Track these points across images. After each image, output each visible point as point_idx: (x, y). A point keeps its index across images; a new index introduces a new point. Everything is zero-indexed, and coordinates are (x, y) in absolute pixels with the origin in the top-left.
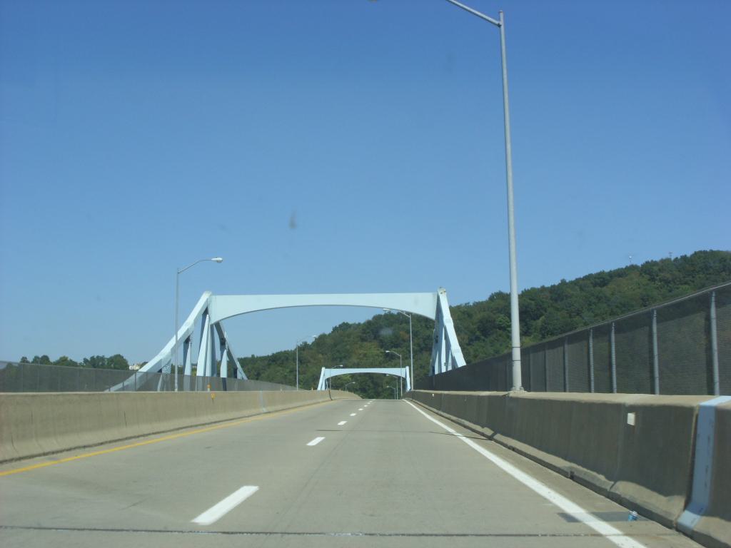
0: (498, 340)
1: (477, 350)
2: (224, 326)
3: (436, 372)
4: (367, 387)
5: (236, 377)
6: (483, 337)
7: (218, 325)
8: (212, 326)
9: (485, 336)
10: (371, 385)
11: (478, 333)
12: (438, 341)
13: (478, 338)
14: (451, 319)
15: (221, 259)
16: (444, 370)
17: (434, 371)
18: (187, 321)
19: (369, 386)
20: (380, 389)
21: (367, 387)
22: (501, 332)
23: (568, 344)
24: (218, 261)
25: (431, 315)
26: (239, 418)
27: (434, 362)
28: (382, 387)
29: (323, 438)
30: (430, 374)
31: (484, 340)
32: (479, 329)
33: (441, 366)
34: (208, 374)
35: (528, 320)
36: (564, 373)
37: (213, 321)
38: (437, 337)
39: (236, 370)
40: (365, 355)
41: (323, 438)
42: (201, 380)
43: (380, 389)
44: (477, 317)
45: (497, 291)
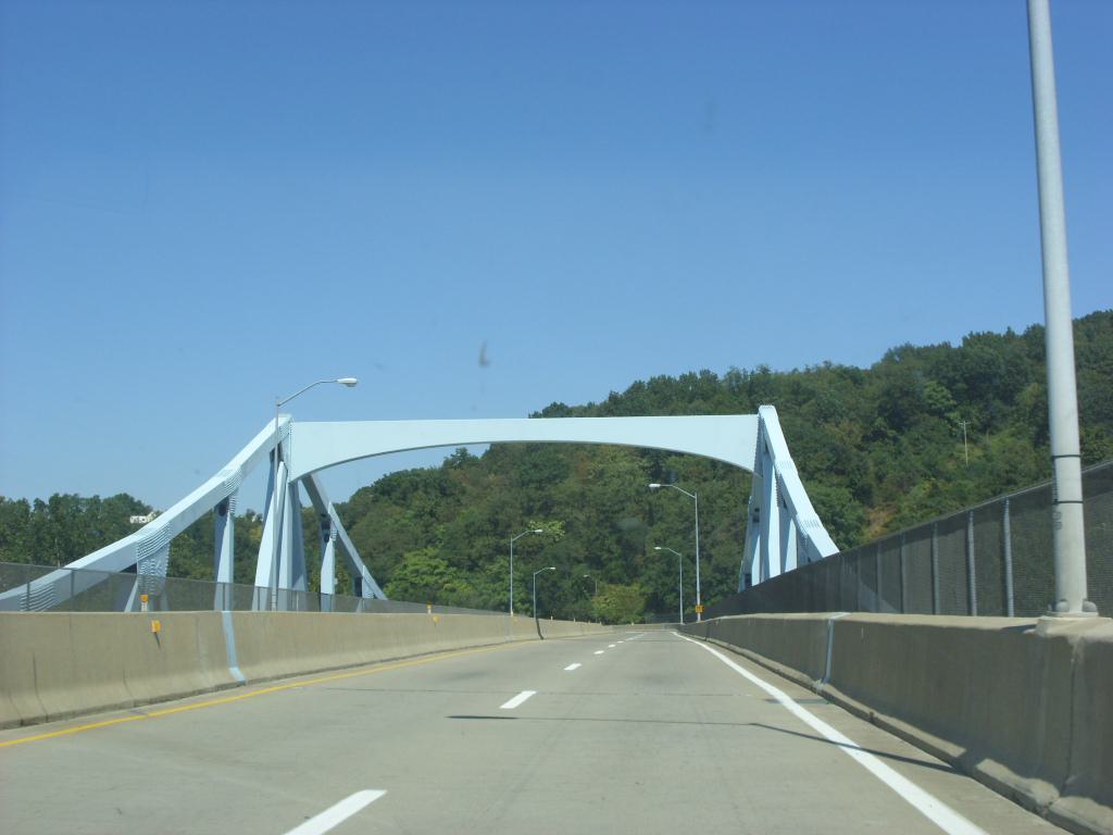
0: (930, 440)
1: (882, 462)
2: (321, 482)
3: (755, 581)
4: (605, 556)
5: (359, 594)
6: (891, 433)
7: (308, 480)
8: (293, 486)
9: (899, 430)
10: (614, 547)
11: (880, 422)
12: (759, 519)
13: (878, 435)
14: (792, 461)
15: (353, 380)
16: (775, 571)
17: (748, 577)
18: (226, 468)
19: (610, 551)
20: (639, 559)
21: (605, 556)
22: (934, 420)
23: (939, 535)
24: (349, 385)
25: (746, 460)
26: (310, 673)
27: (749, 565)
28: (644, 553)
29: (503, 707)
30: (741, 587)
31: (895, 440)
32: (882, 410)
33: (774, 558)
34: (284, 583)
35: (991, 396)
36: (933, 583)
37: (297, 472)
38: (757, 510)
39: (358, 581)
40: (601, 474)
41: (503, 707)
42: (264, 595)
43: (639, 559)
44: (872, 389)
45: (900, 343)
